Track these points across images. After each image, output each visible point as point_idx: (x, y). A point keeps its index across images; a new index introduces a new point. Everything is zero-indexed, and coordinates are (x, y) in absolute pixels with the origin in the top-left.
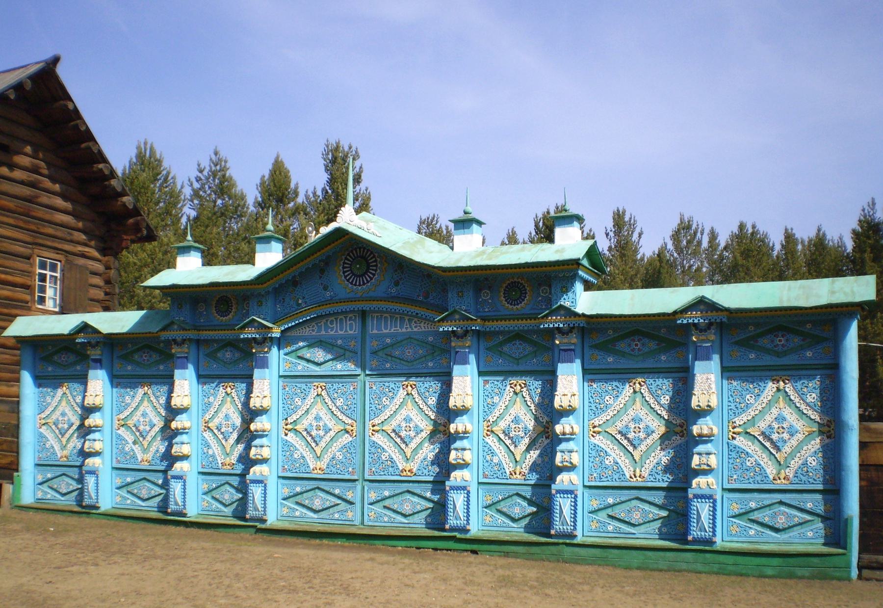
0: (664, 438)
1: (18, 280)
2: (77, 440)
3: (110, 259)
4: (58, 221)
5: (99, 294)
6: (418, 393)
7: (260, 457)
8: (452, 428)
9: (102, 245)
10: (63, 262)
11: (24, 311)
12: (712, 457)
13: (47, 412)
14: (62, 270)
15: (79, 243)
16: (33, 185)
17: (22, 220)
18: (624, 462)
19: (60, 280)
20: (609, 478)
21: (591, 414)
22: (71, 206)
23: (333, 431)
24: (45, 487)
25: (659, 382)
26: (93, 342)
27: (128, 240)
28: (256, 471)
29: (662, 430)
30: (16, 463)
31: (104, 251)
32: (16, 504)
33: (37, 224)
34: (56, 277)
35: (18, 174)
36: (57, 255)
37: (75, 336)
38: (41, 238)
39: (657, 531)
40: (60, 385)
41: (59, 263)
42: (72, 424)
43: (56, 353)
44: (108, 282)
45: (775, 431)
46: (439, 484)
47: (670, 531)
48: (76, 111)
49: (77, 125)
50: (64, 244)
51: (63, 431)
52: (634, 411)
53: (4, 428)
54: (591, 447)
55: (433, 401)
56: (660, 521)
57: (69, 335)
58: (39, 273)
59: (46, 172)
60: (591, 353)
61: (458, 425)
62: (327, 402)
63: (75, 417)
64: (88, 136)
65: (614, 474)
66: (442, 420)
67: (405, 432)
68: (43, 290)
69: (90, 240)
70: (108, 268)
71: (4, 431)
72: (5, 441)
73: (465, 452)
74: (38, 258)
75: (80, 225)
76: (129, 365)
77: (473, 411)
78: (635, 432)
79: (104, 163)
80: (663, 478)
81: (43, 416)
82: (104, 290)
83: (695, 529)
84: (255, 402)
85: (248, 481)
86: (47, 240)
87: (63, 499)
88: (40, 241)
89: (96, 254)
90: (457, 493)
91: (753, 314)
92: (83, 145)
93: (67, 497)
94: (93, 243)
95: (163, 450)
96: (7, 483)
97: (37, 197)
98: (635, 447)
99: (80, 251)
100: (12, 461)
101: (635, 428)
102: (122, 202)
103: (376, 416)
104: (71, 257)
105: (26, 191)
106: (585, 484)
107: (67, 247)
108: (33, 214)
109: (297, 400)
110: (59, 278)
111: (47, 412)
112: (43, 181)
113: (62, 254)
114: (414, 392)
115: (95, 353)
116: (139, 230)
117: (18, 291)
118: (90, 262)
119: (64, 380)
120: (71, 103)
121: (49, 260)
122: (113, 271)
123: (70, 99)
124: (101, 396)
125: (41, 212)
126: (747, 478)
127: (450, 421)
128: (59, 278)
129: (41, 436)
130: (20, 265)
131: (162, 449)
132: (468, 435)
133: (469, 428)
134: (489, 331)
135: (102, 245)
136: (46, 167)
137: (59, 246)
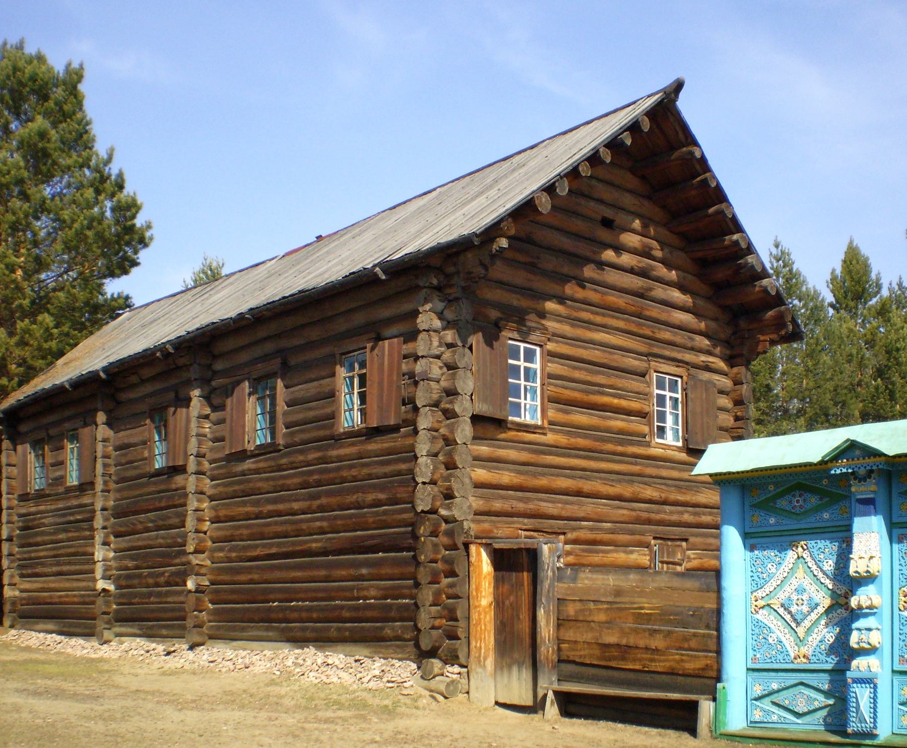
0: (828, 611)
1: (635, 405)
2: (826, 630)
3: (740, 370)
4: (677, 322)
5: (727, 420)
6: (811, 556)
7: (866, 646)
8: (854, 602)
9: (728, 352)
10: (685, 378)
11: (641, 448)
12: (874, 633)
13: (768, 588)
14: (684, 389)
15: (701, 351)
16: (643, 273)
17: (634, 322)
18: (788, 641)
19: (682, 402)
20: (773, 660)
21: (902, 579)
22: (690, 300)
23: (822, 606)
24: (766, 704)
25: (821, 544)
26: (862, 472)
27: (766, 341)
28: (860, 664)
29: (827, 602)
30: (715, 667)
31: (731, 361)
32: (722, 730)
33: (652, 327)
34: (677, 399)
35: (626, 259)
36: (676, 369)
37: (830, 465)
38: (658, 347)
39: (821, 721)
40: (792, 545)
41: (679, 380)
42: (817, 605)
43: (781, 495)
44: (739, 402)
45: (794, 602)
46: (839, 674)
47: (836, 721)
48: (703, 160)
49: (706, 179)
50: (685, 353)
51: (798, 617)
52: (797, 580)
53: (692, 615)
54: (754, 623)
55: (829, 565)
56: (827, 709)
57: (822, 462)
58: (657, 394)
59: (658, 254)
60: (751, 513)
61: (861, 597)
62: (810, 566)
63: (821, 594)
64: (719, 196)
65: (778, 655)
66: (842, 590)
67: (796, 606)
68: (662, 417)
69: (714, 346)
70: (737, 383)
71: (691, 619)
72: (695, 635)
73: (871, 632)
74: (655, 374)
75: (702, 325)
76: (770, 516)
77: (881, 580)
78: (797, 604)
79: (738, 233)
80: (827, 659)
81: (760, 593)
82: (734, 414)
83: (854, 719)
84: (856, 566)
85: (849, 680)
86: (665, 348)
87: (799, 721)
88: (656, 350)
89: (722, 365)
90: (862, 687)
91: (778, 471)
92: (712, 210)
93: (807, 719)
94: (718, 350)
95: (832, 640)
96: (707, 699)
97: (651, 289)
98: (798, 624)
99: (703, 361)
100: (707, 665)
101: (798, 599)
102: (761, 286)
103: (759, 586)
104: (693, 371)
105: (636, 282)
106: (895, 669)
107: (688, 357)
108: (647, 313)
109: (769, 566)
110: (680, 400)
111: (768, 588)
112: (655, 267)
113: (683, 367)
114: (806, 555)
115: (860, 490)
116: (784, 325)
117: (632, 421)
118: (716, 377)
119: (800, 537)
120: (698, 149)
121: (668, 377)
122: (745, 386)
123: (695, 143)
124: (877, 558)
125: (655, 311)
126: (769, 656)
127: (852, 592)
128: (680, 400)
129: (758, 624)
130: (634, 384)
131: (830, 638)
132: (875, 610)
133: (876, 601)
134: (834, 474)
135: (728, 352)
136: (659, 248)
137: (679, 356)
